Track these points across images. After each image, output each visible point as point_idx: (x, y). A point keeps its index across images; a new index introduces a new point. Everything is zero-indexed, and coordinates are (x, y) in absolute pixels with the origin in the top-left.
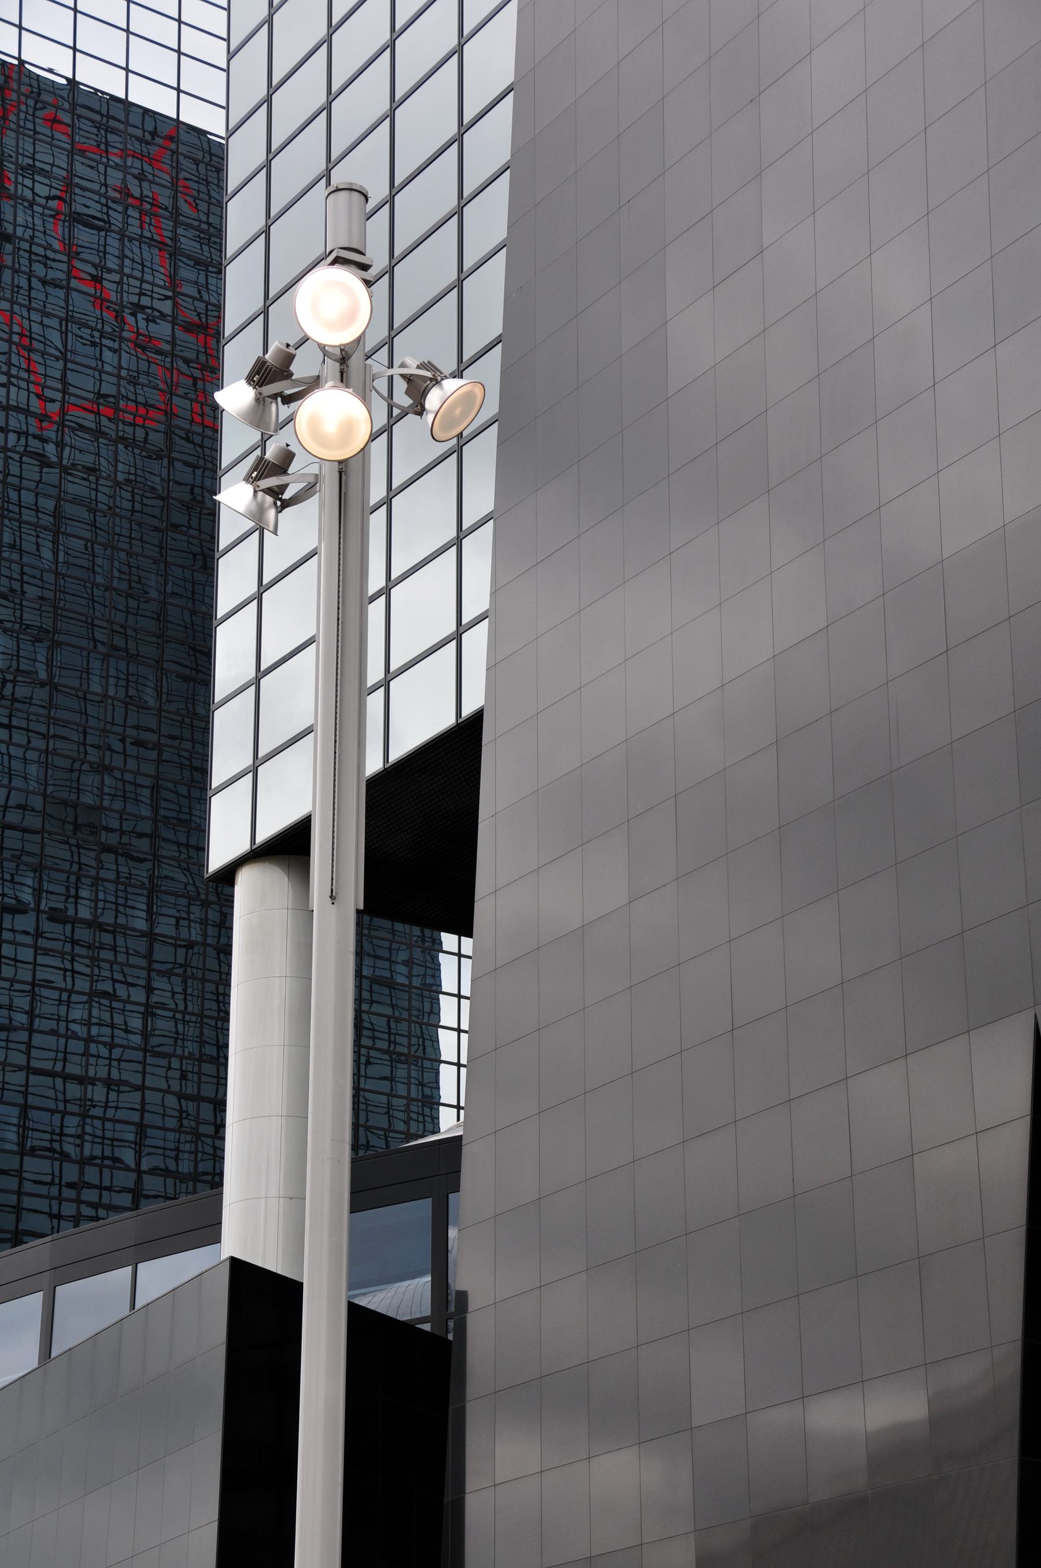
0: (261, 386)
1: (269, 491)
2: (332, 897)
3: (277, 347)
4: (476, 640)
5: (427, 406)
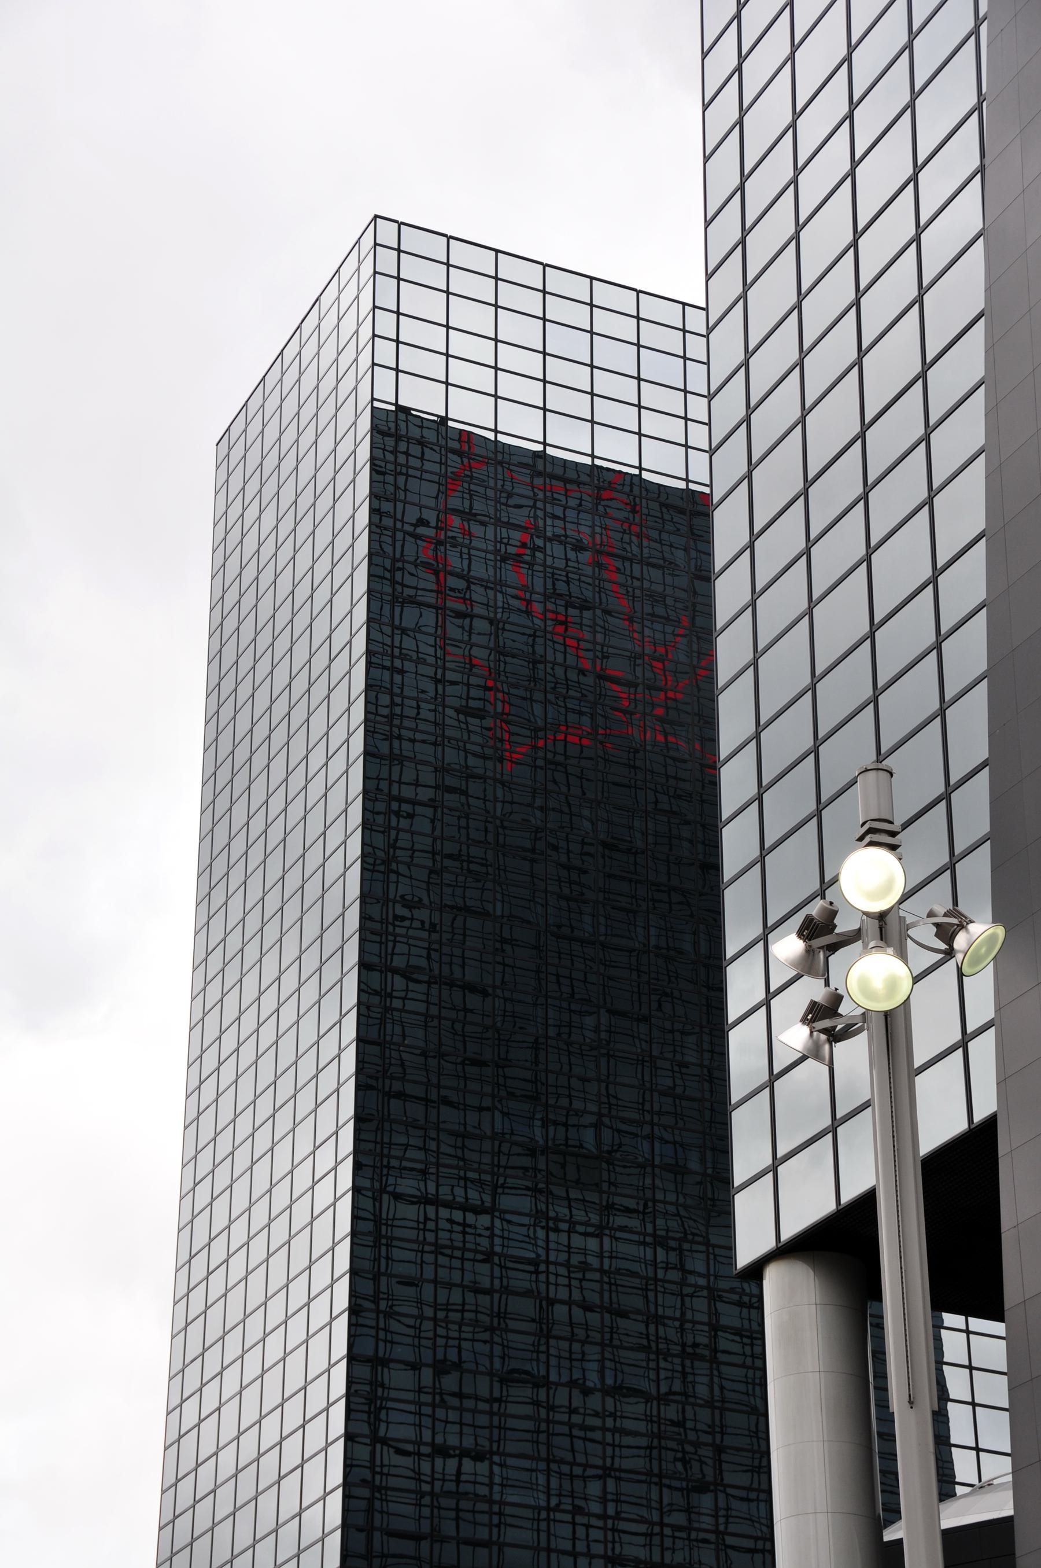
0: (810, 940)
1: (824, 1031)
2: (911, 1402)
3: (822, 905)
4: (984, 1049)
5: (956, 946)
